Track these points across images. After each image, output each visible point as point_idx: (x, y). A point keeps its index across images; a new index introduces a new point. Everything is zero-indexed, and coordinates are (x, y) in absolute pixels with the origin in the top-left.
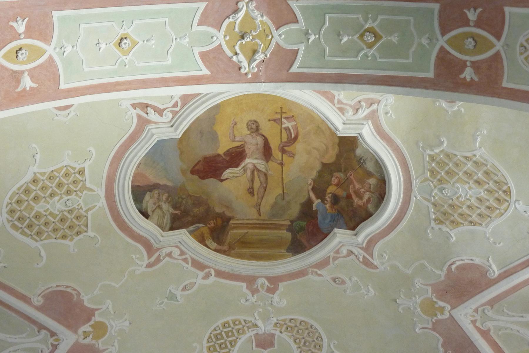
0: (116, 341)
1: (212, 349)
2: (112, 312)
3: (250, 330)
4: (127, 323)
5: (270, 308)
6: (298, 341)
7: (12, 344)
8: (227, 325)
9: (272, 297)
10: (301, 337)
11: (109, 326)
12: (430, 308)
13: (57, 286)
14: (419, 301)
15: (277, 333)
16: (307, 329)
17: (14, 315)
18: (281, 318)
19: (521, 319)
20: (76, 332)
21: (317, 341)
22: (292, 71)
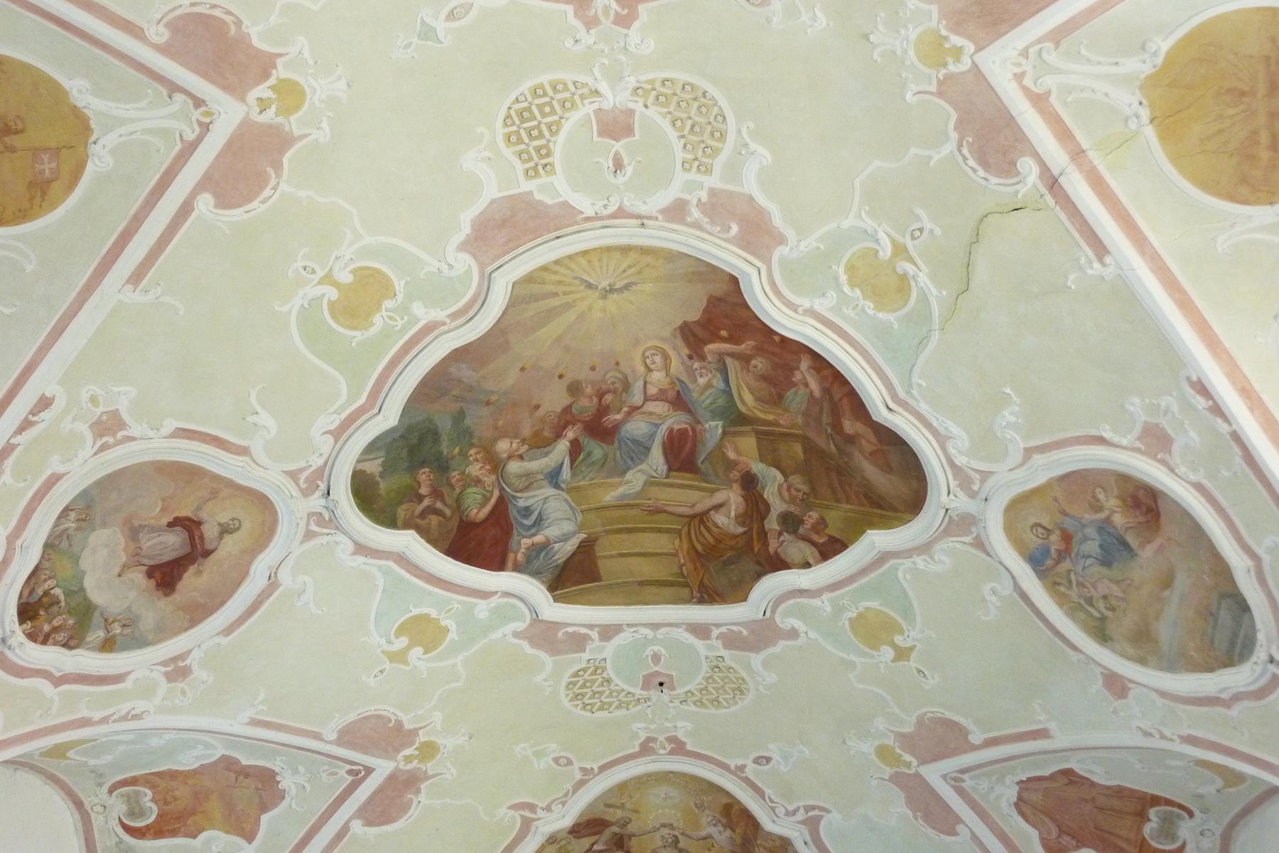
0: (325, 119)
1: (513, 139)
2: (311, 62)
3: (586, 101)
4: (342, 85)
5: (623, 58)
6: (679, 123)
7: (122, 122)
8: (540, 92)
9: (626, 35)
10: (685, 115)
11: (307, 90)
12: (934, 50)
13: (193, 5)
14: (913, 36)
15: (638, 107)
16: (695, 99)
17: (116, 62)
18: (644, 78)
19: (1114, 70)
20: (242, 99)
21: (715, 124)
22: (925, 771)
